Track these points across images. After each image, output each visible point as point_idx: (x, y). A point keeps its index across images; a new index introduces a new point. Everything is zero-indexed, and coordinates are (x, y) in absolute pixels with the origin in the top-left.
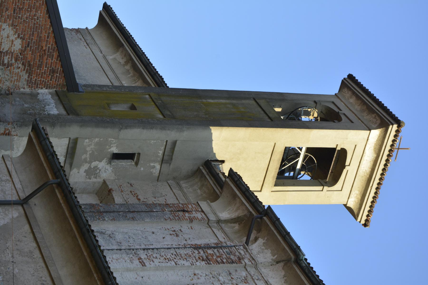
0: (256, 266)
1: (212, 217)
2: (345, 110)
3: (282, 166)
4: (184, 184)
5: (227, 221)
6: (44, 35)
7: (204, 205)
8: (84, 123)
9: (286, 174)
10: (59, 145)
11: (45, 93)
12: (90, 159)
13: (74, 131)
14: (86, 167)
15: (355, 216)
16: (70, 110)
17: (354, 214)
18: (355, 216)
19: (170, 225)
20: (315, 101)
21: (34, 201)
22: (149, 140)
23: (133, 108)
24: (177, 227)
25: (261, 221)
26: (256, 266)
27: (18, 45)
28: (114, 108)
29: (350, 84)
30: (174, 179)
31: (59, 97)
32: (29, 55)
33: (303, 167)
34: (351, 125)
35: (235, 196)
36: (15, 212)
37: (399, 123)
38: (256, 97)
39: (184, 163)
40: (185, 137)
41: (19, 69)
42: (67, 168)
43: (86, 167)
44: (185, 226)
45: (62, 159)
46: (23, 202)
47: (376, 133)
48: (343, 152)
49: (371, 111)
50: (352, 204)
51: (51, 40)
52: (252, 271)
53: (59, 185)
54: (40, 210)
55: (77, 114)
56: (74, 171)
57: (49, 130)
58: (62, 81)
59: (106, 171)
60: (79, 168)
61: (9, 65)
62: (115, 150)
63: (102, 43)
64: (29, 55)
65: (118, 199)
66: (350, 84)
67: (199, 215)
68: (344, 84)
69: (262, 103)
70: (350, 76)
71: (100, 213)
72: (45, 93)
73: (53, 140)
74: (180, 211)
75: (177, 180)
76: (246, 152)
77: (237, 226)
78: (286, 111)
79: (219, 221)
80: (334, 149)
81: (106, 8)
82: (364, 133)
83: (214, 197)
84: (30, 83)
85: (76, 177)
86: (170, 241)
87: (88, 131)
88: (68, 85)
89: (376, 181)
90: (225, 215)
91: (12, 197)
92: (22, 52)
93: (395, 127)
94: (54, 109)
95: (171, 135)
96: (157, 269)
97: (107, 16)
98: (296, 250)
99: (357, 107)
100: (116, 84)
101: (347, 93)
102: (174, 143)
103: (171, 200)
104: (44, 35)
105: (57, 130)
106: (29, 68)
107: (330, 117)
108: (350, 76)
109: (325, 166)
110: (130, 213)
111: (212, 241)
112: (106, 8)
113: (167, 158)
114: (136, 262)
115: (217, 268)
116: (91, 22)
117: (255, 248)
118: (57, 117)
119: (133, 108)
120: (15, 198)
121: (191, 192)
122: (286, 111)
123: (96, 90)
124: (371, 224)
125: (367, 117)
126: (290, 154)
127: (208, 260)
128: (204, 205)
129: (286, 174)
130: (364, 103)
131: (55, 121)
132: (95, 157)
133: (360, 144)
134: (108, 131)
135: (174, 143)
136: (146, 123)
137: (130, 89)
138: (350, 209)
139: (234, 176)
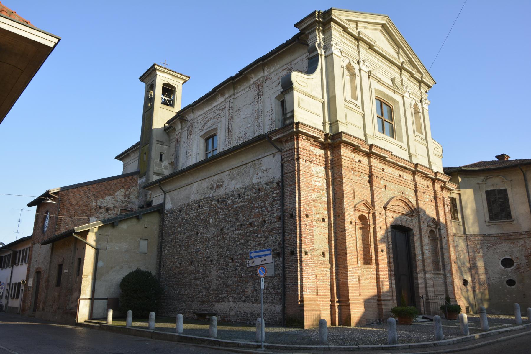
0: (194, 119)
1: (180, 131)
2: (150, 82)
3: (168, 105)
4: (171, 138)
5: (182, 126)
6: (119, 182)
7: (177, 133)
8: (149, 170)
9: (170, 103)
10: (156, 178)
11: (139, 182)
12: (160, 168)
13: (151, 173)
14: (164, 170)
15: (186, 81)
16: (145, 174)
17: (186, 81)
18: (186, 81)
19: (181, 145)
20: (147, 92)
21: (164, 190)
22: (156, 149)
23: (145, 153)
24: (182, 143)
25: (181, 116)
26: (194, 119)
27: (123, 190)
28: (145, 160)
29: (142, 79)
30: (169, 141)
31: (141, 177)
32: (126, 186)
33: (169, 97)
34: (155, 81)
35: (174, 123)
36: (167, 196)
37: (154, 65)
38: (145, 112)
39: (164, 138)
40: (155, 138)
41: (131, 190)
42: (164, 176)
43: (164, 170)
44: (182, 140)
45: (160, 177)
46: (165, 193)
47: (158, 73)
48: (164, 84)
49: (150, 73)
50: (182, 82)
51: (121, 179)
52: (195, 120)
53: (160, 182)
54: (167, 188)
55: (146, 172)
56: (165, 173)
57: (150, 182)
58: (135, 176)
59: (165, 163)
60: (164, 172)
61: (129, 193)
62: (158, 160)
63: (128, 160)
64: (126, 186)
65: (173, 160)
66: (142, 79)
67: (179, 135)
68: (142, 81)
69: (146, 110)
70: (140, 78)
71: (176, 167)
72: (139, 182)
73: (154, 180)
74: (178, 141)
75: (170, 140)
76: (162, 116)
77: (183, 123)
78: (149, 101)
79: (181, 129)
80: (163, 87)
81: (116, 158)
82: (158, 77)
83: (174, 129)
84: (136, 186)
85: (167, 172)
86: (185, 146)
87: (151, 169)
88: (138, 174)
89: (175, 74)
90: (180, 127)
91: (163, 196)
92: (125, 189)
93: (156, 66)
94: (144, 179)
95: (154, 142)
96: (192, 151)
97: (119, 158)
98: (189, 106)
99: (150, 78)
100: (138, 158)
101: (145, 80)
102: (157, 141)
103: (174, 143)
104: (119, 182)
105: (150, 179)
106: (130, 187)
107: (151, 87)
108: (140, 78)
109: (168, 90)
110: (177, 157)
111: (187, 131)
112: (116, 158)
113: (162, 143)
114: (190, 157)
115: (194, 132)
116: (121, 163)
117: (189, 119)
118: (146, 178)
119: (145, 153)
120: (163, 195)
121: (173, 136)
122: (149, 101)
123: (139, 165)
124: (189, 76)
125: (153, 75)
126: (164, 103)
127: (191, 134)
128: (177, 133)
129: (170, 103)
130: (146, 77)
131: (148, 179)
132: (161, 167)
133: (161, 78)
134: (152, 162)
135: (157, 141)
136: (150, 150)
137: (140, 154)
138: (184, 83)
139: (168, 122)
